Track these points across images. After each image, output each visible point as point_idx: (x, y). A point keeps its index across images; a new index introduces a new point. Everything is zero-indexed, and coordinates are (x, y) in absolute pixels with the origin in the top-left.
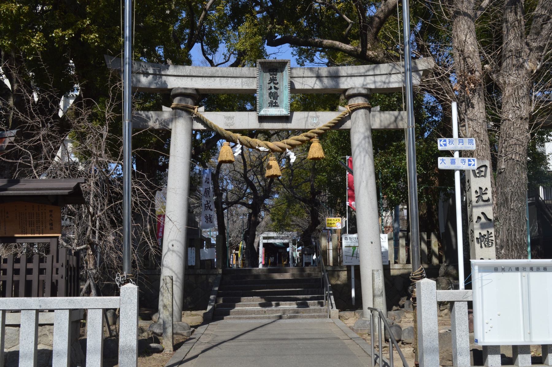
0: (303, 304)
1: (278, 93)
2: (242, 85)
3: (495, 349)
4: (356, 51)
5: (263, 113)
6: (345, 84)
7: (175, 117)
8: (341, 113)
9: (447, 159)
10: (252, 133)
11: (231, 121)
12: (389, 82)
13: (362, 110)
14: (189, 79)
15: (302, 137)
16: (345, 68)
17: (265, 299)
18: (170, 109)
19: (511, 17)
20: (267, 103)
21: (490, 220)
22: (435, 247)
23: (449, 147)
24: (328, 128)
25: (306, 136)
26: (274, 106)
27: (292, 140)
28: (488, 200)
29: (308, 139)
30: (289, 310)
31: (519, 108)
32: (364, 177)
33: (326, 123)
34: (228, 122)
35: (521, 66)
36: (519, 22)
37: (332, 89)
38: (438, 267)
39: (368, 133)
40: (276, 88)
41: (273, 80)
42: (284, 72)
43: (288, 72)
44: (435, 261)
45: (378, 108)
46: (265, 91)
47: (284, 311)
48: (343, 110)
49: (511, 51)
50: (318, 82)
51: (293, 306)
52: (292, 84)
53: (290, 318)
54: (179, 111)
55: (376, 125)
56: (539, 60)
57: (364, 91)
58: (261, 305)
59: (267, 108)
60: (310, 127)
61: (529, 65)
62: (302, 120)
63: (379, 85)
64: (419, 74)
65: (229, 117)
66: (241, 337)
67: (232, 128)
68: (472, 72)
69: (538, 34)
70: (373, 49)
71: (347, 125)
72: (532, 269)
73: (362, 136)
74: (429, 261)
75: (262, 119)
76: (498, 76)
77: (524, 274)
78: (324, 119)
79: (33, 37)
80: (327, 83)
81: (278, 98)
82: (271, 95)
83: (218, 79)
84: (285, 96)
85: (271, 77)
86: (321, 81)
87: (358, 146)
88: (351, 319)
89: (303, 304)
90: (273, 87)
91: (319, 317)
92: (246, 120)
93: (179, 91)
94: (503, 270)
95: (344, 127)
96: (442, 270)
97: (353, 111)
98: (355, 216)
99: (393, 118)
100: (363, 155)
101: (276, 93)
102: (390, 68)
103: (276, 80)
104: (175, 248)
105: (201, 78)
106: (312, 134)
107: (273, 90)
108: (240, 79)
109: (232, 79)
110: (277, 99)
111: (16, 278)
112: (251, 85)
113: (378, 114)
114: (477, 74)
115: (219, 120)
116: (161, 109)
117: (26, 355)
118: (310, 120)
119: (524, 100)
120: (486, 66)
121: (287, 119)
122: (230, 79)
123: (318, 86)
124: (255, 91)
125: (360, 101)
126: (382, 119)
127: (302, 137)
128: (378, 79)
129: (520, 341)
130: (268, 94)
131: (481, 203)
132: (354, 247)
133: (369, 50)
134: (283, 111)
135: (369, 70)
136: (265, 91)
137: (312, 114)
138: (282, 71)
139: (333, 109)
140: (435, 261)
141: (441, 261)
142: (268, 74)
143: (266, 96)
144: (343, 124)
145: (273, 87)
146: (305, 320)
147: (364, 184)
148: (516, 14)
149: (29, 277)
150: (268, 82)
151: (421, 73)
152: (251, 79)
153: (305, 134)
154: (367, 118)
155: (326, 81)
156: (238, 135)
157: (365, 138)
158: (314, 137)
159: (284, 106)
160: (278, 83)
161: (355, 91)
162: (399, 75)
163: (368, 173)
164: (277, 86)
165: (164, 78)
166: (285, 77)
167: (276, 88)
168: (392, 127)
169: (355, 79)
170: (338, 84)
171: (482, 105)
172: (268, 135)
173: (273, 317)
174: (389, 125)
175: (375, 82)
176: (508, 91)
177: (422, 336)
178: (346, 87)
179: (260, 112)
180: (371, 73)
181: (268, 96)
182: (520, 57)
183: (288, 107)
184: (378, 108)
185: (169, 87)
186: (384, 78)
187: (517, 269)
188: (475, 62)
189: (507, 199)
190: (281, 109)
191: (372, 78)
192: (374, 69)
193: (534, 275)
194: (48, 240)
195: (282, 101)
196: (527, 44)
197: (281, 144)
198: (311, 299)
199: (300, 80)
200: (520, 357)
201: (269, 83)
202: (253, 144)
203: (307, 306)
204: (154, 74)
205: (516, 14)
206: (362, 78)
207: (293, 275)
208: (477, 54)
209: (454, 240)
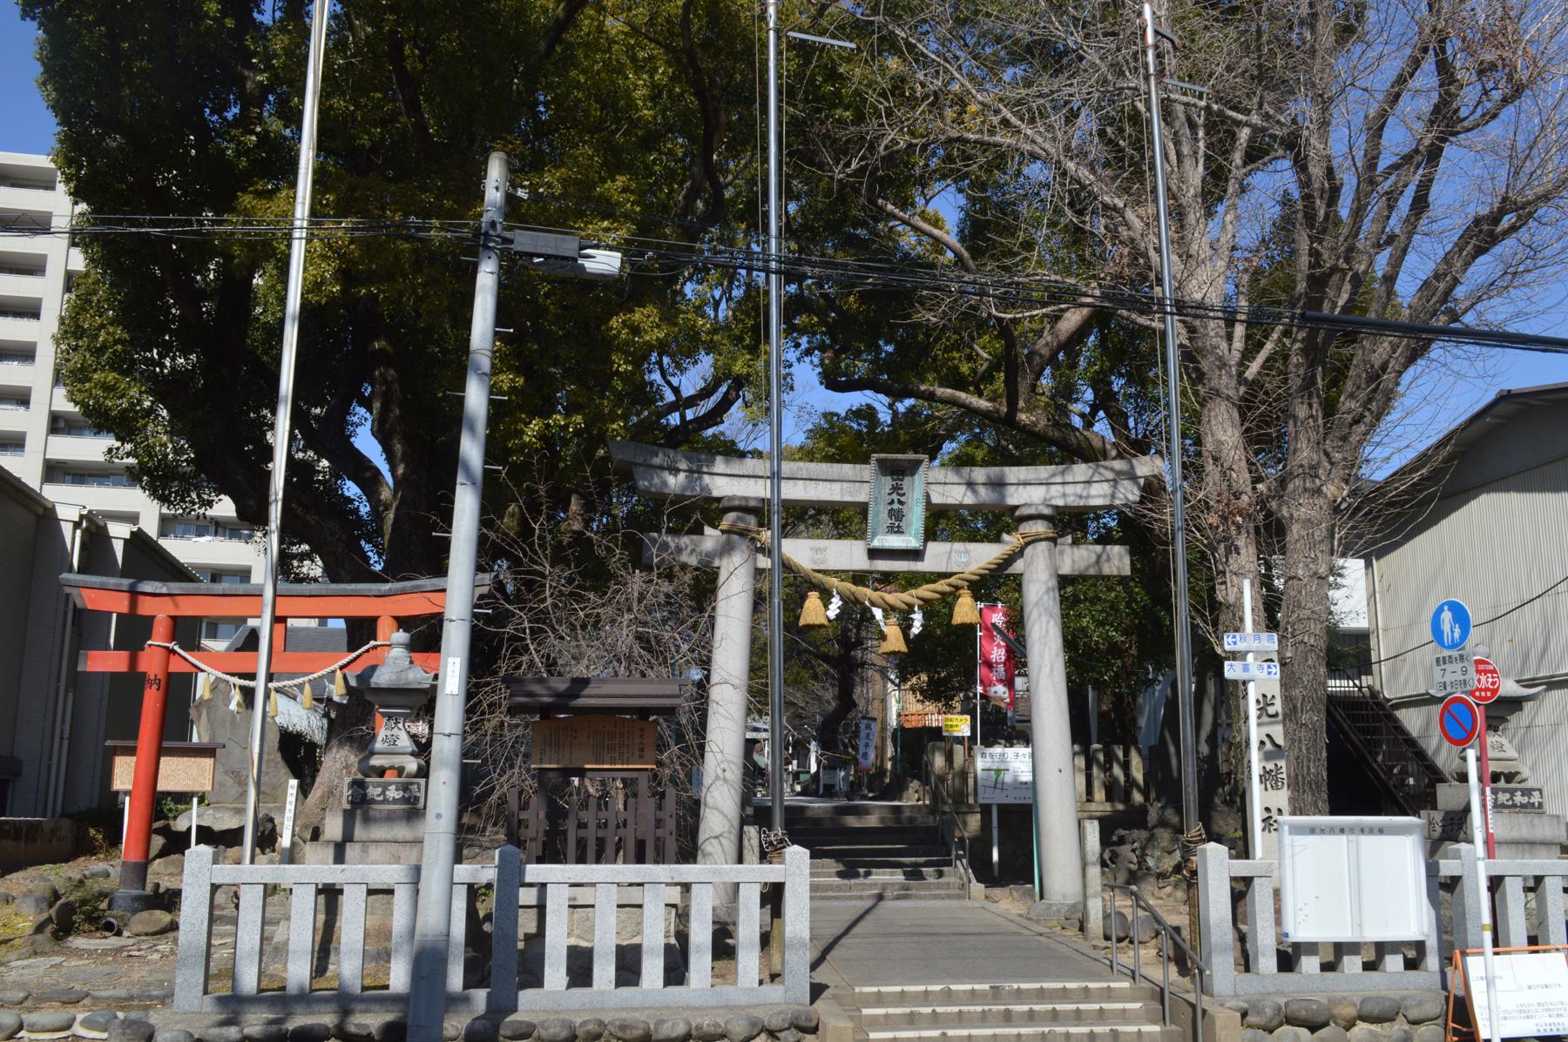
0: (914, 874)
3: (1312, 948)
4: (997, 411)
6: (1015, 497)
7: (727, 549)
9: (1238, 664)
10: (859, 578)
12: (1088, 497)
13: (1044, 544)
14: (752, 481)
15: (942, 586)
16: (1015, 469)
17: (845, 864)
18: (716, 533)
19: (1301, 411)
21: (1278, 746)
22: (1138, 775)
23: (1241, 646)
28: (1276, 715)
30: (893, 884)
31: (1315, 560)
32: (1046, 657)
33: (982, 564)
35: (1318, 491)
36: (1315, 420)
37: (993, 505)
38: (1143, 811)
39: (1053, 583)
40: (900, 502)
41: (896, 489)
44: (1138, 797)
45: (1069, 539)
47: (885, 886)
48: (1011, 541)
49: (1301, 466)
50: (969, 493)
51: (898, 877)
52: (928, 496)
53: (898, 898)
54: (735, 537)
55: (1066, 569)
56: (1347, 482)
57: (1047, 511)
58: (840, 874)
60: (955, 570)
61: (1330, 490)
62: (940, 555)
63: (1072, 501)
64: (1138, 484)
66: (856, 930)
67: (822, 567)
68: (1237, 496)
69: (1344, 439)
70: (1029, 410)
71: (1018, 567)
72: (1362, 831)
73: (1044, 588)
74: (1127, 798)
75: (874, 554)
76: (1280, 506)
77: (1352, 837)
78: (979, 556)
79: (527, 424)
80: (985, 494)
84: (916, 517)
86: (974, 492)
87: (1037, 604)
88: (1007, 903)
89: (914, 874)
91: (949, 897)
92: (847, 554)
93: (737, 503)
94: (1323, 832)
95: (1011, 570)
96: (1153, 815)
97: (1027, 544)
98: (1074, 742)
99: (1094, 558)
100: (1044, 619)
101: (900, 511)
102: (1090, 472)
104: (728, 775)
106: (960, 583)
107: (896, 506)
111: (582, 833)
112: (861, 495)
113: (1068, 550)
114: (1245, 498)
115: (803, 552)
116: (701, 533)
117: (652, 950)
118: (954, 556)
119: (1323, 547)
120: (1260, 486)
121: (916, 555)
123: (969, 499)
125: (1040, 527)
126: (1076, 558)
127: (942, 586)
128: (1070, 489)
129: (1346, 935)
131: (1265, 719)
132: (998, 771)
133: (1022, 411)
134: (910, 541)
135: (1054, 475)
137: (958, 546)
138: (912, 475)
139: (997, 539)
140: (1138, 797)
141: (1147, 799)
143: (884, 515)
146: (922, 903)
147: (1046, 671)
148: (1310, 406)
149: (660, 832)
151: (1142, 481)
154: (1051, 556)
155: (982, 491)
156: (835, 581)
157: (1047, 592)
161: (1032, 511)
162: (1105, 485)
163: (1054, 652)
165: (707, 479)
167: (900, 502)
168: (1092, 572)
169: (1033, 489)
170: (1003, 497)
171: (1252, 550)
172: (887, 579)
173: (869, 897)
174: (1087, 568)
175: (1064, 495)
176: (1295, 531)
177: (1209, 928)
178: (1016, 503)
180: (1058, 479)
182: (1317, 476)
184: (1069, 539)
185: (716, 494)
186: (1079, 489)
187: (1342, 831)
188: (1242, 478)
189: (1295, 707)
191: (1059, 487)
192: (1063, 473)
193: (1366, 840)
194: (635, 775)
195: (910, 525)
196: (1327, 454)
198: (927, 864)
199: (940, 488)
200: (1346, 958)
202: (860, 597)
203: (921, 877)
204: (690, 471)
205: (1310, 406)
206: (1043, 488)
207: (882, 820)
208: (1243, 464)
209: (1174, 761)
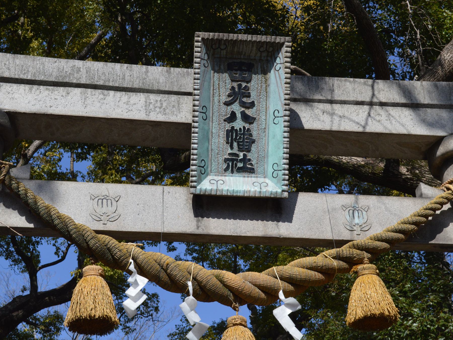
1: (254, 133)
2: (148, 112)
5: (207, 185)
8: (427, 203)
11: (110, 210)
15: (325, 258)
20: (221, 159)
24: (401, 236)
25: (337, 257)
26: (241, 170)
27: (296, 267)
29: (343, 264)
34: (100, 210)
40: (247, 118)
41: (239, 95)
42: (272, 75)
43: (282, 72)
46: (215, 124)
59: (218, 173)
60: (345, 235)
62: (322, 214)
65: (106, 198)
67: (112, 227)
75: (205, 205)
81: (254, 148)
82: (232, 136)
83: (78, 91)
84: (273, 146)
85: (235, 85)
90: (239, 115)
92: (158, 207)
103: (249, 96)
105: (27, 87)
107: (239, 124)
108: (142, 97)
109: (119, 94)
110: (249, 151)
121: (275, 208)
122: (112, 93)
124: (185, 129)
127: (325, 258)
130: (223, 134)
134: (268, 183)
136: (215, 124)
138: (265, 71)
139: (408, 189)
142: (226, 76)
144: (440, 231)
145: (239, 115)
150: (224, 98)
152: (174, 98)
153: (333, 251)
158: (360, 262)
159: (270, 170)
160: (252, 105)
164: (249, 112)
166: (273, 87)
167: (247, 118)
179: (199, 181)
181: (222, 140)
183: (283, 174)
190: (261, 180)
195: (263, 158)
197: (263, 277)
201: (227, 104)
